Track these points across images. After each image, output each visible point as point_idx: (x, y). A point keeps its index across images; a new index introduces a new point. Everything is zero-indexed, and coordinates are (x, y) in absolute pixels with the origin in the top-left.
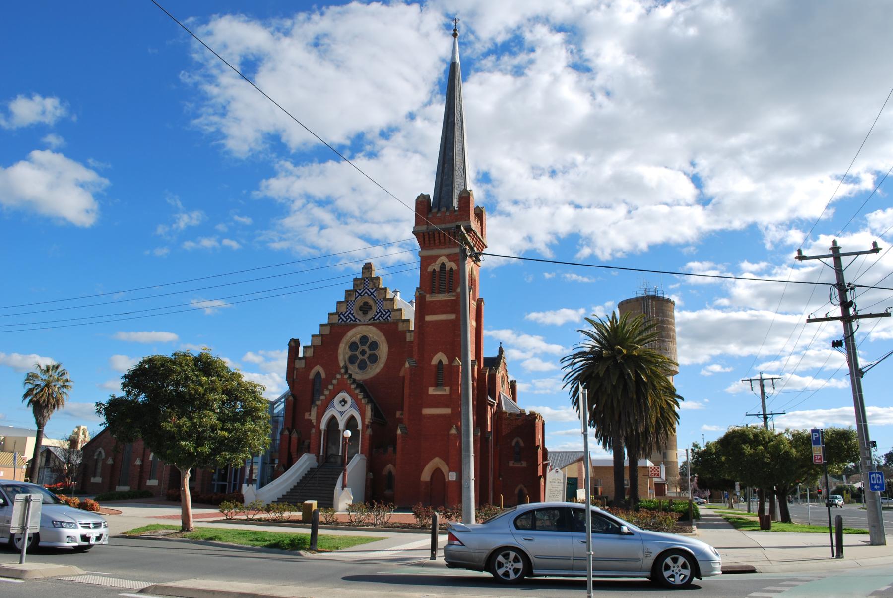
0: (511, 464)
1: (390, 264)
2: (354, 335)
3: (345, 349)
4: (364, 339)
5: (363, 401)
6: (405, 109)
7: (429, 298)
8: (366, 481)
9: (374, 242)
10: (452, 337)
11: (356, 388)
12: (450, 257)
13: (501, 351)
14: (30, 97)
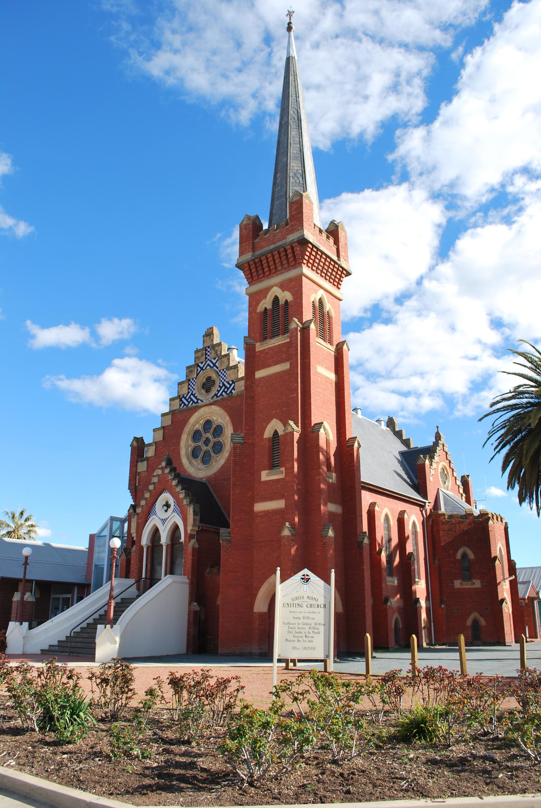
0: (457, 584)
1: (423, 411)
2: (195, 421)
3: (187, 440)
4: (208, 423)
5: (185, 502)
6: (414, 277)
7: (259, 347)
8: (189, 615)
9: (406, 394)
10: (294, 394)
11: (177, 486)
12: (283, 286)
13: (438, 437)
14: (110, 319)
